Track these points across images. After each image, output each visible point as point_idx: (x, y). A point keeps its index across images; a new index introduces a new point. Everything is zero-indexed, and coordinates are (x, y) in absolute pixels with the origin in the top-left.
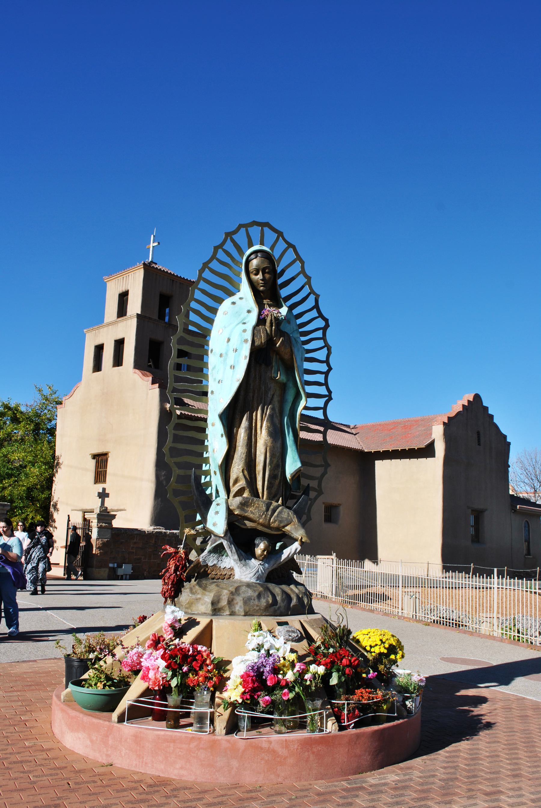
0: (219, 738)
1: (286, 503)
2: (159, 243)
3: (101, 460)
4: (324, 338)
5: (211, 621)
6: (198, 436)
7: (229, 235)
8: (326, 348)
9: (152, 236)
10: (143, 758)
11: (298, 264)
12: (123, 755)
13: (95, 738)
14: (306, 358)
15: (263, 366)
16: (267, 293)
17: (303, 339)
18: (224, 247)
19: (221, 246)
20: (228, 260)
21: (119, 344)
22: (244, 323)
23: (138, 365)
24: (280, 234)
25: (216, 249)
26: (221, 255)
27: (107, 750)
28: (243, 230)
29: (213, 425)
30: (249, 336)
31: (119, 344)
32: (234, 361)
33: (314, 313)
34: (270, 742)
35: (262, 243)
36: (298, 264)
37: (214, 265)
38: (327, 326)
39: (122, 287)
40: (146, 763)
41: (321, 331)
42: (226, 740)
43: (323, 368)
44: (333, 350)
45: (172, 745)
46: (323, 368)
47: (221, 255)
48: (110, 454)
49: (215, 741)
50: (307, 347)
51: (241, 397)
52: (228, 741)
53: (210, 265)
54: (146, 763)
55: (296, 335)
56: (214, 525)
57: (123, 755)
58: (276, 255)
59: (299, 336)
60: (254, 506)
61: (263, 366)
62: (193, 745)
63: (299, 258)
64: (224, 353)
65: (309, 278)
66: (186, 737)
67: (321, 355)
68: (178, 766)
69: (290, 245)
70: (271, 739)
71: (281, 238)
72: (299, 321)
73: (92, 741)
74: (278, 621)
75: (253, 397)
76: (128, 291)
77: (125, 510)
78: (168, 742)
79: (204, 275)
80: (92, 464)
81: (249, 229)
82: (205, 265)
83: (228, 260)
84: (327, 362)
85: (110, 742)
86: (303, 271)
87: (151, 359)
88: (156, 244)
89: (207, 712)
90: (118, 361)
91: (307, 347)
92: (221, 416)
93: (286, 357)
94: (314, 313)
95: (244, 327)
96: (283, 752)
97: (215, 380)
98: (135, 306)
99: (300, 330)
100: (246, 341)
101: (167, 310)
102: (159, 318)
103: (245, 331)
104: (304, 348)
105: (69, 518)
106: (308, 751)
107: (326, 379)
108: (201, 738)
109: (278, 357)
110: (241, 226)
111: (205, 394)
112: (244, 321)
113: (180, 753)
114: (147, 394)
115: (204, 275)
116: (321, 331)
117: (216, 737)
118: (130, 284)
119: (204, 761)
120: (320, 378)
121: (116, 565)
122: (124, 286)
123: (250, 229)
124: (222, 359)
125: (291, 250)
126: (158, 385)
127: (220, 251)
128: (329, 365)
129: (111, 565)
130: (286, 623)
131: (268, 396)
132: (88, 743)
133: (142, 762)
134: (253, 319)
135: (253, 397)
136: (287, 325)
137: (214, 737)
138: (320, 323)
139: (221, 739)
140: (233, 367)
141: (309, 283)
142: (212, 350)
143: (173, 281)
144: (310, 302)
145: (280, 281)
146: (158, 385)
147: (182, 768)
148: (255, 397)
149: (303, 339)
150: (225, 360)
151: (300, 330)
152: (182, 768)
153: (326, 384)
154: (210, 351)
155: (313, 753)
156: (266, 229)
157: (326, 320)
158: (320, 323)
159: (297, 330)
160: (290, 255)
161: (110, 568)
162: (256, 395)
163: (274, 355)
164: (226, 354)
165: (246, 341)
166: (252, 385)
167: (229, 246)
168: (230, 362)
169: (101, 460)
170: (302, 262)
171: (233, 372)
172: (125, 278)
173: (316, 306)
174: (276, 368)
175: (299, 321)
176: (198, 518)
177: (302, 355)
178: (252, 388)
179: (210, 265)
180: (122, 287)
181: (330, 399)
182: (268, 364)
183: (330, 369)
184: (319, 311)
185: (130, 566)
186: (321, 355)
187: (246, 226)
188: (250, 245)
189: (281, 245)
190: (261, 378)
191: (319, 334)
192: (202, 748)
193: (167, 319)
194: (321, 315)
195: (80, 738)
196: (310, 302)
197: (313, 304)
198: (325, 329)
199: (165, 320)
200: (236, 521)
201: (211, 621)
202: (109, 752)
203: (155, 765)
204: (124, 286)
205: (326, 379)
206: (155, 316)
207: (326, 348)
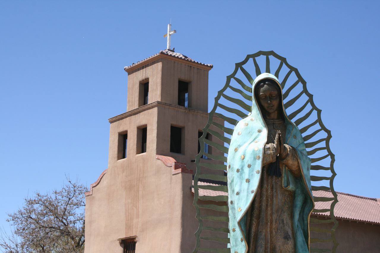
2: (175, 31)
4: (327, 148)
6: (223, 219)
8: (330, 156)
9: (169, 25)
11: (300, 86)
14: (312, 166)
15: (274, 177)
16: (275, 117)
17: (308, 150)
18: (235, 76)
19: (233, 76)
20: (239, 87)
21: (143, 131)
23: (160, 152)
24: (283, 60)
25: (229, 78)
26: (233, 83)
28: (251, 60)
29: (234, 230)
31: (143, 131)
32: (249, 176)
33: (317, 127)
35: (268, 71)
38: (330, 136)
41: (325, 142)
43: (329, 174)
44: (336, 158)
46: (329, 174)
47: (233, 83)
50: (311, 157)
51: (256, 205)
53: (225, 93)
55: (301, 148)
59: (305, 148)
63: (301, 79)
64: (240, 168)
65: (311, 96)
67: (326, 163)
69: (292, 69)
71: (284, 64)
72: (304, 135)
79: (220, 102)
81: (256, 58)
83: (239, 87)
84: (332, 168)
86: (305, 91)
87: (174, 142)
88: (172, 32)
90: (142, 147)
91: (311, 157)
92: (239, 223)
93: (294, 168)
94: (317, 127)
97: (233, 191)
98: (155, 95)
99: (306, 142)
101: (186, 95)
104: (309, 158)
107: (331, 184)
109: (287, 168)
111: (226, 184)
114: (171, 179)
115: (220, 102)
116: (325, 142)
124: (239, 174)
126: (180, 169)
127: (232, 80)
136: (294, 140)
138: (323, 135)
140: (248, 181)
142: (230, 166)
143: (190, 67)
144: (314, 117)
145: (285, 102)
146: (180, 169)
149: (308, 150)
150: (241, 174)
151: (306, 142)
154: (228, 168)
156: (271, 57)
157: (328, 132)
158: (323, 135)
159: (303, 143)
160: (293, 78)
164: (242, 169)
165: (252, 192)
167: (240, 75)
168: (246, 176)
170: (304, 83)
171: (249, 184)
173: (319, 121)
175: (304, 135)
179: (225, 93)
180: (142, 76)
182: (279, 175)
183: (334, 174)
184: (321, 125)
187: (254, 56)
188: (258, 73)
191: (323, 144)
193: (186, 104)
194: (323, 128)
196: (314, 117)
199: (184, 106)
205: (331, 184)
207: (330, 156)
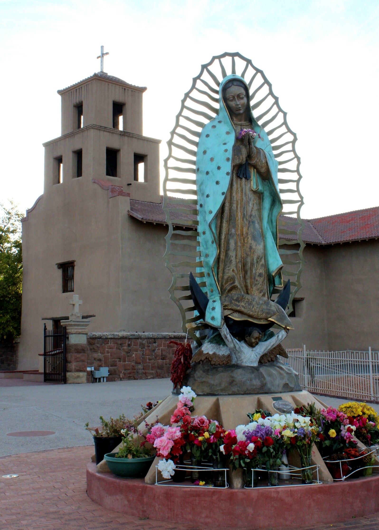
0: (236, 490)
1: (270, 297)
3: (67, 268)
4: (294, 150)
5: (218, 400)
7: (204, 67)
10: (174, 511)
12: (157, 510)
13: (131, 498)
19: (199, 77)
22: (225, 144)
24: (249, 62)
25: (195, 80)
27: (143, 507)
30: (230, 154)
34: (278, 492)
36: (266, 87)
37: (195, 94)
38: (295, 139)
39: (76, 99)
40: (177, 515)
42: (242, 492)
43: (295, 176)
45: (197, 498)
46: (295, 176)
48: (75, 263)
49: (233, 494)
52: (244, 493)
53: (190, 95)
54: (177, 515)
56: (213, 318)
57: (157, 510)
58: (247, 80)
60: (244, 301)
61: (244, 180)
62: (214, 498)
63: (266, 82)
65: (276, 99)
66: (209, 491)
67: (292, 165)
68: (203, 516)
69: (258, 71)
70: (279, 490)
73: (129, 501)
74: (273, 397)
75: (237, 207)
76: (82, 102)
77: (94, 316)
78: (194, 496)
80: (59, 273)
82: (187, 95)
84: (298, 171)
85: (145, 500)
86: (271, 93)
89: (224, 471)
94: (284, 129)
95: (225, 147)
96: (288, 500)
100: (228, 159)
102: (114, 127)
103: (226, 151)
105: (45, 327)
106: (310, 499)
108: (221, 491)
110: (214, 58)
112: (225, 142)
113: (204, 505)
115: (186, 104)
117: (233, 490)
118: (83, 95)
119: (225, 510)
120: (293, 186)
121: (93, 369)
122: (78, 97)
123: (222, 60)
125: (259, 75)
127: (198, 81)
128: (299, 174)
129: (89, 369)
130: (280, 398)
131: (249, 206)
132: (126, 502)
133: (173, 514)
134: (231, 140)
135: (237, 207)
137: (231, 490)
138: (289, 137)
139: (238, 492)
141: (276, 103)
144: (280, 119)
147: (207, 517)
148: (239, 207)
149: (275, 152)
152: (207, 517)
153: (298, 191)
155: (314, 500)
157: (294, 135)
158: (290, 138)
161: (88, 372)
162: (239, 205)
163: (252, 170)
166: (235, 197)
169: (67, 268)
170: (270, 85)
172: (78, 91)
173: (285, 123)
174: (255, 180)
175: (271, 137)
176: (5, 337)
177: (276, 166)
178: (235, 199)
180: (76, 99)
181: (302, 203)
185: (107, 369)
186: (292, 165)
187: (219, 57)
189: (251, 72)
190: (242, 190)
191: (289, 147)
192: (222, 500)
194: (289, 131)
195: (118, 500)
196: (280, 119)
197: (282, 121)
198: (294, 142)
200: (229, 315)
201: (218, 400)
202: (145, 509)
203: (184, 516)
204: (78, 97)
206: (111, 126)
